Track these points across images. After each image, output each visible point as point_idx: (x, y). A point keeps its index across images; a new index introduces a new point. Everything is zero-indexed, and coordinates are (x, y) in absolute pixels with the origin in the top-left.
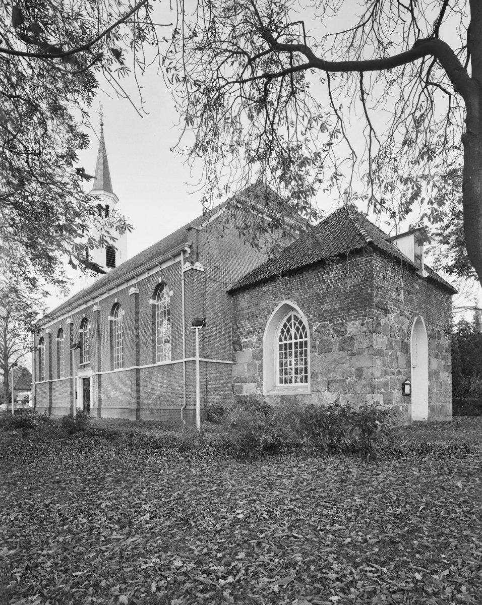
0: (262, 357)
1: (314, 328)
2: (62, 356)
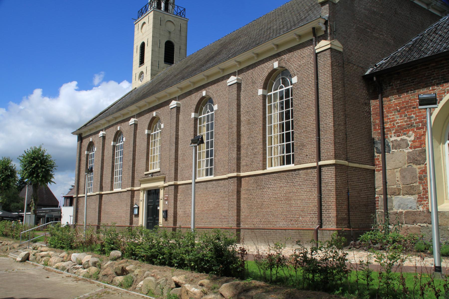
0: (425, 159)
2: (118, 163)
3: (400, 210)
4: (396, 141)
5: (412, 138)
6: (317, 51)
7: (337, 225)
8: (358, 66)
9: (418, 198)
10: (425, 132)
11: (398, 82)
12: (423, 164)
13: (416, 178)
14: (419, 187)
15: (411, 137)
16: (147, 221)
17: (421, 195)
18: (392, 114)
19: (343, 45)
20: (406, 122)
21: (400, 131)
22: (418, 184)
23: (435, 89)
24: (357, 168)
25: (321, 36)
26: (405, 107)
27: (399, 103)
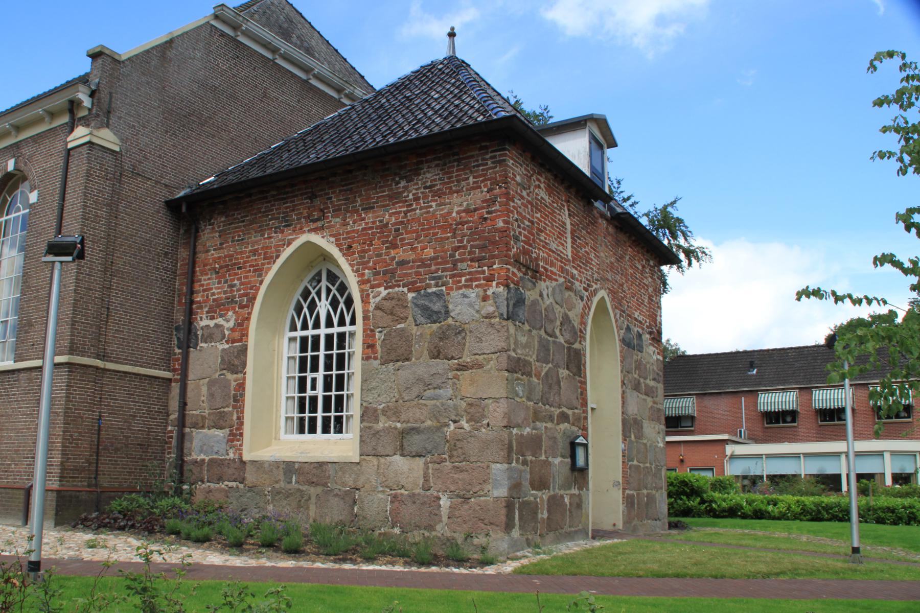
0: (244, 364)
3: (202, 456)
4: (208, 326)
5: (231, 324)
6: (70, 146)
7: (60, 481)
8: (157, 182)
9: (229, 435)
10: (250, 314)
11: (223, 219)
12: (241, 372)
13: (229, 398)
14: (231, 413)
15: (228, 323)
16: (50, 416)
18: (206, 277)
19: (122, 140)
20: (225, 292)
21: (217, 309)
22: (230, 409)
24: (129, 373)
25: (83, 117)
26: (227, 266)
27: (219, 258)
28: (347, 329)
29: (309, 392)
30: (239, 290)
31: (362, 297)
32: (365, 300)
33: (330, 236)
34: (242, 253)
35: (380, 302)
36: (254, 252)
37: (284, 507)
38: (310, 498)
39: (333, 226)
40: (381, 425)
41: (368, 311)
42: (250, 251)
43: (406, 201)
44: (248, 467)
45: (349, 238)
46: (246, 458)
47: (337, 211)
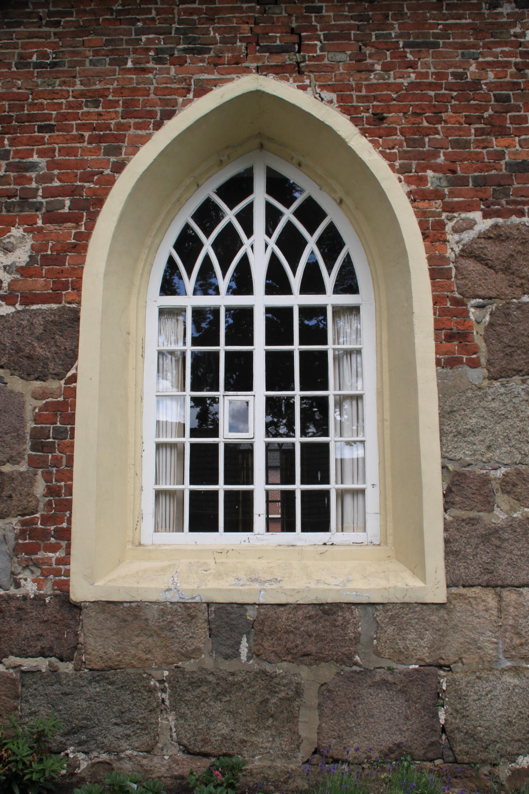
0: (72, 356)
1: (454, 243)
9: (22, 534)
12: (59, 376)
13: (20, 438)
14: (28, 480)
17: (33, 522)
22: (23, 467)
23: (145, 71)
28: (329, 299)
29: (226, 435)
30: (41, 179)
31: (423, 225)
32: (432, 233)
33: (323, 87)
34: (54, 94)
35: (474, 241)
36: (95, 97)
37: (212, 719)
38: (298, 693)
39: (331, 68)
40: (499, 516)
41: (444, 259)
42: (82, 94)
43: (520, 44)
44: (89, 621)
45: (375, 98)
46: (80, 591)
47: (336, 37)
